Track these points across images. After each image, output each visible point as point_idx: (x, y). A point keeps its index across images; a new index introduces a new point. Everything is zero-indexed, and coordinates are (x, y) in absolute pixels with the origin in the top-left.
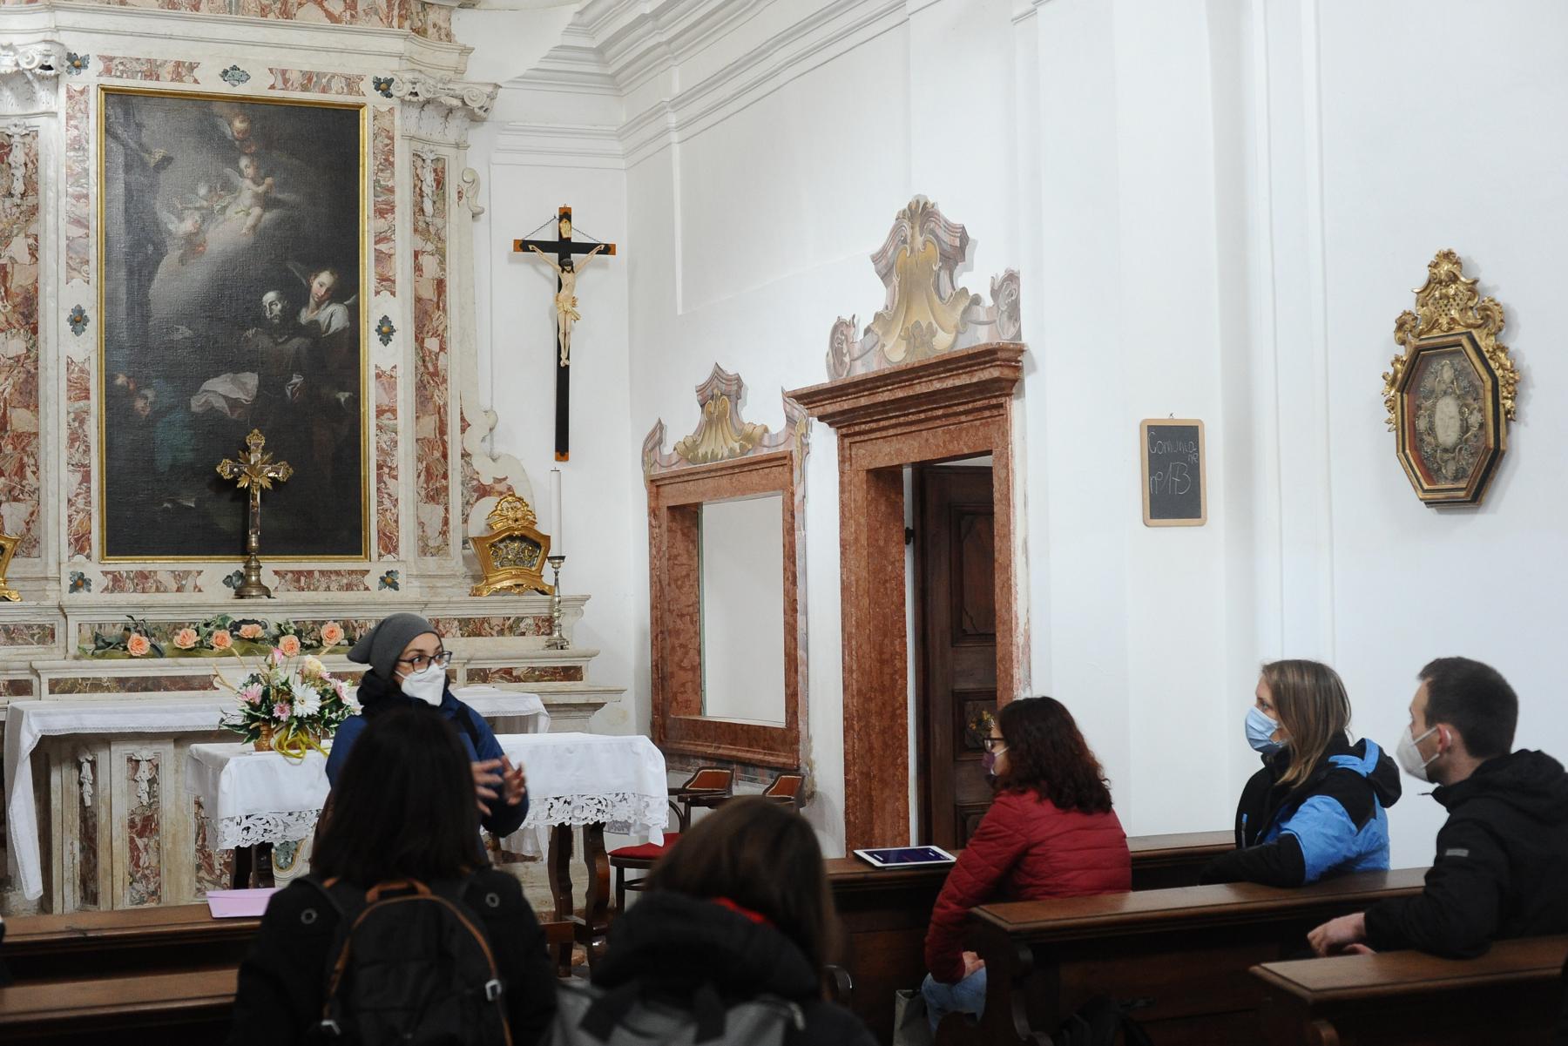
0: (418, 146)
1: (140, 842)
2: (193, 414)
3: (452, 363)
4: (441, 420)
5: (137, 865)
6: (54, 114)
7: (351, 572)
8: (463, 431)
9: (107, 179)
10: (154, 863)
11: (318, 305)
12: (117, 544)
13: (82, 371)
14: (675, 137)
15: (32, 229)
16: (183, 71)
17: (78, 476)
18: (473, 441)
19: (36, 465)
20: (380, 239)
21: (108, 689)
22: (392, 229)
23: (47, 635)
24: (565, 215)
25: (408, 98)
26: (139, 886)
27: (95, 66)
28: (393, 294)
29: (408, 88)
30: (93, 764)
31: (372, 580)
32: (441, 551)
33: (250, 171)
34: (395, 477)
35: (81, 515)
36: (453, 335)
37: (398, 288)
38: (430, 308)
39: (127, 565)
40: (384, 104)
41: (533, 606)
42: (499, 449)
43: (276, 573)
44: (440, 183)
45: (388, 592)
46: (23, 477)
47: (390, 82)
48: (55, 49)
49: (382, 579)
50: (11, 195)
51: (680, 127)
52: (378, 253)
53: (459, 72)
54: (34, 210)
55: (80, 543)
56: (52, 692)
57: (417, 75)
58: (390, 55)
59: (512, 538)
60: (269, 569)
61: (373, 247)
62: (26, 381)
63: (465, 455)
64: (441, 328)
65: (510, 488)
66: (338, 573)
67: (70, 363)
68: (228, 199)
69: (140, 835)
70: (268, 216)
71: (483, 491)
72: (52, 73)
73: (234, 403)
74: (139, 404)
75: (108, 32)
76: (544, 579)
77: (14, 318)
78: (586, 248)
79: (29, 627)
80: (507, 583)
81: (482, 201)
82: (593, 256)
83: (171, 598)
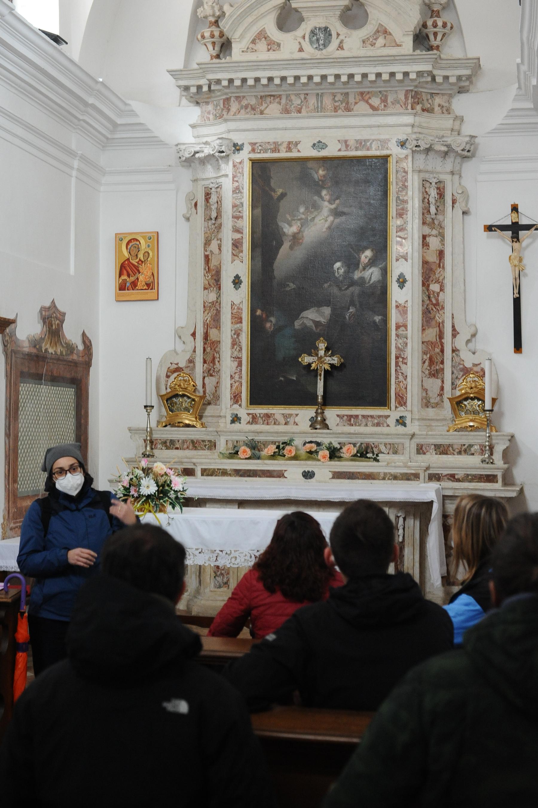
2: (295, 329)
4: (440, 331)
6: (226, 176)
7: (379, 417)
9: (254, 207)
11: (364, 269)
12: (256, 399)
13: (238, 308)
15: (219, 237)
16: (292, 146)
17: (236, 364)
18: (460, 342)
19: (219, 358)
21: (230, 475)
22: (406, 223)
23: (212, 445)
24: (515, 209)
25: (414, 149)
26: (219, 579)
27: (247, 148)
29: (415, 143)
31: (392, 421)
33: (327, 197)
34: (406, 364)
35: (237, 384)
36: (448, 283)
38: (434, 267)
41: (478, 438)
43: (338, 416)
44: (441, 195)
45: (400, 428)
46: (214, 364)
48: (225, 142)
49: (397, 420)
50: (211, 219)
55: (236, 398)
56: (202, 475)
57: (418, 135)
58: (406, 125)
60: (332, 414)
62: (216, 314)
63: (454, 351)
66: (372, 417)
68: (316, 213)
70: (337, 221)
72: (224, 154)
73: (317, 324)
74: (268, 325)
75: (258, 130)
77: (212, 282)
78: (528, 227)
83: (281, 428)
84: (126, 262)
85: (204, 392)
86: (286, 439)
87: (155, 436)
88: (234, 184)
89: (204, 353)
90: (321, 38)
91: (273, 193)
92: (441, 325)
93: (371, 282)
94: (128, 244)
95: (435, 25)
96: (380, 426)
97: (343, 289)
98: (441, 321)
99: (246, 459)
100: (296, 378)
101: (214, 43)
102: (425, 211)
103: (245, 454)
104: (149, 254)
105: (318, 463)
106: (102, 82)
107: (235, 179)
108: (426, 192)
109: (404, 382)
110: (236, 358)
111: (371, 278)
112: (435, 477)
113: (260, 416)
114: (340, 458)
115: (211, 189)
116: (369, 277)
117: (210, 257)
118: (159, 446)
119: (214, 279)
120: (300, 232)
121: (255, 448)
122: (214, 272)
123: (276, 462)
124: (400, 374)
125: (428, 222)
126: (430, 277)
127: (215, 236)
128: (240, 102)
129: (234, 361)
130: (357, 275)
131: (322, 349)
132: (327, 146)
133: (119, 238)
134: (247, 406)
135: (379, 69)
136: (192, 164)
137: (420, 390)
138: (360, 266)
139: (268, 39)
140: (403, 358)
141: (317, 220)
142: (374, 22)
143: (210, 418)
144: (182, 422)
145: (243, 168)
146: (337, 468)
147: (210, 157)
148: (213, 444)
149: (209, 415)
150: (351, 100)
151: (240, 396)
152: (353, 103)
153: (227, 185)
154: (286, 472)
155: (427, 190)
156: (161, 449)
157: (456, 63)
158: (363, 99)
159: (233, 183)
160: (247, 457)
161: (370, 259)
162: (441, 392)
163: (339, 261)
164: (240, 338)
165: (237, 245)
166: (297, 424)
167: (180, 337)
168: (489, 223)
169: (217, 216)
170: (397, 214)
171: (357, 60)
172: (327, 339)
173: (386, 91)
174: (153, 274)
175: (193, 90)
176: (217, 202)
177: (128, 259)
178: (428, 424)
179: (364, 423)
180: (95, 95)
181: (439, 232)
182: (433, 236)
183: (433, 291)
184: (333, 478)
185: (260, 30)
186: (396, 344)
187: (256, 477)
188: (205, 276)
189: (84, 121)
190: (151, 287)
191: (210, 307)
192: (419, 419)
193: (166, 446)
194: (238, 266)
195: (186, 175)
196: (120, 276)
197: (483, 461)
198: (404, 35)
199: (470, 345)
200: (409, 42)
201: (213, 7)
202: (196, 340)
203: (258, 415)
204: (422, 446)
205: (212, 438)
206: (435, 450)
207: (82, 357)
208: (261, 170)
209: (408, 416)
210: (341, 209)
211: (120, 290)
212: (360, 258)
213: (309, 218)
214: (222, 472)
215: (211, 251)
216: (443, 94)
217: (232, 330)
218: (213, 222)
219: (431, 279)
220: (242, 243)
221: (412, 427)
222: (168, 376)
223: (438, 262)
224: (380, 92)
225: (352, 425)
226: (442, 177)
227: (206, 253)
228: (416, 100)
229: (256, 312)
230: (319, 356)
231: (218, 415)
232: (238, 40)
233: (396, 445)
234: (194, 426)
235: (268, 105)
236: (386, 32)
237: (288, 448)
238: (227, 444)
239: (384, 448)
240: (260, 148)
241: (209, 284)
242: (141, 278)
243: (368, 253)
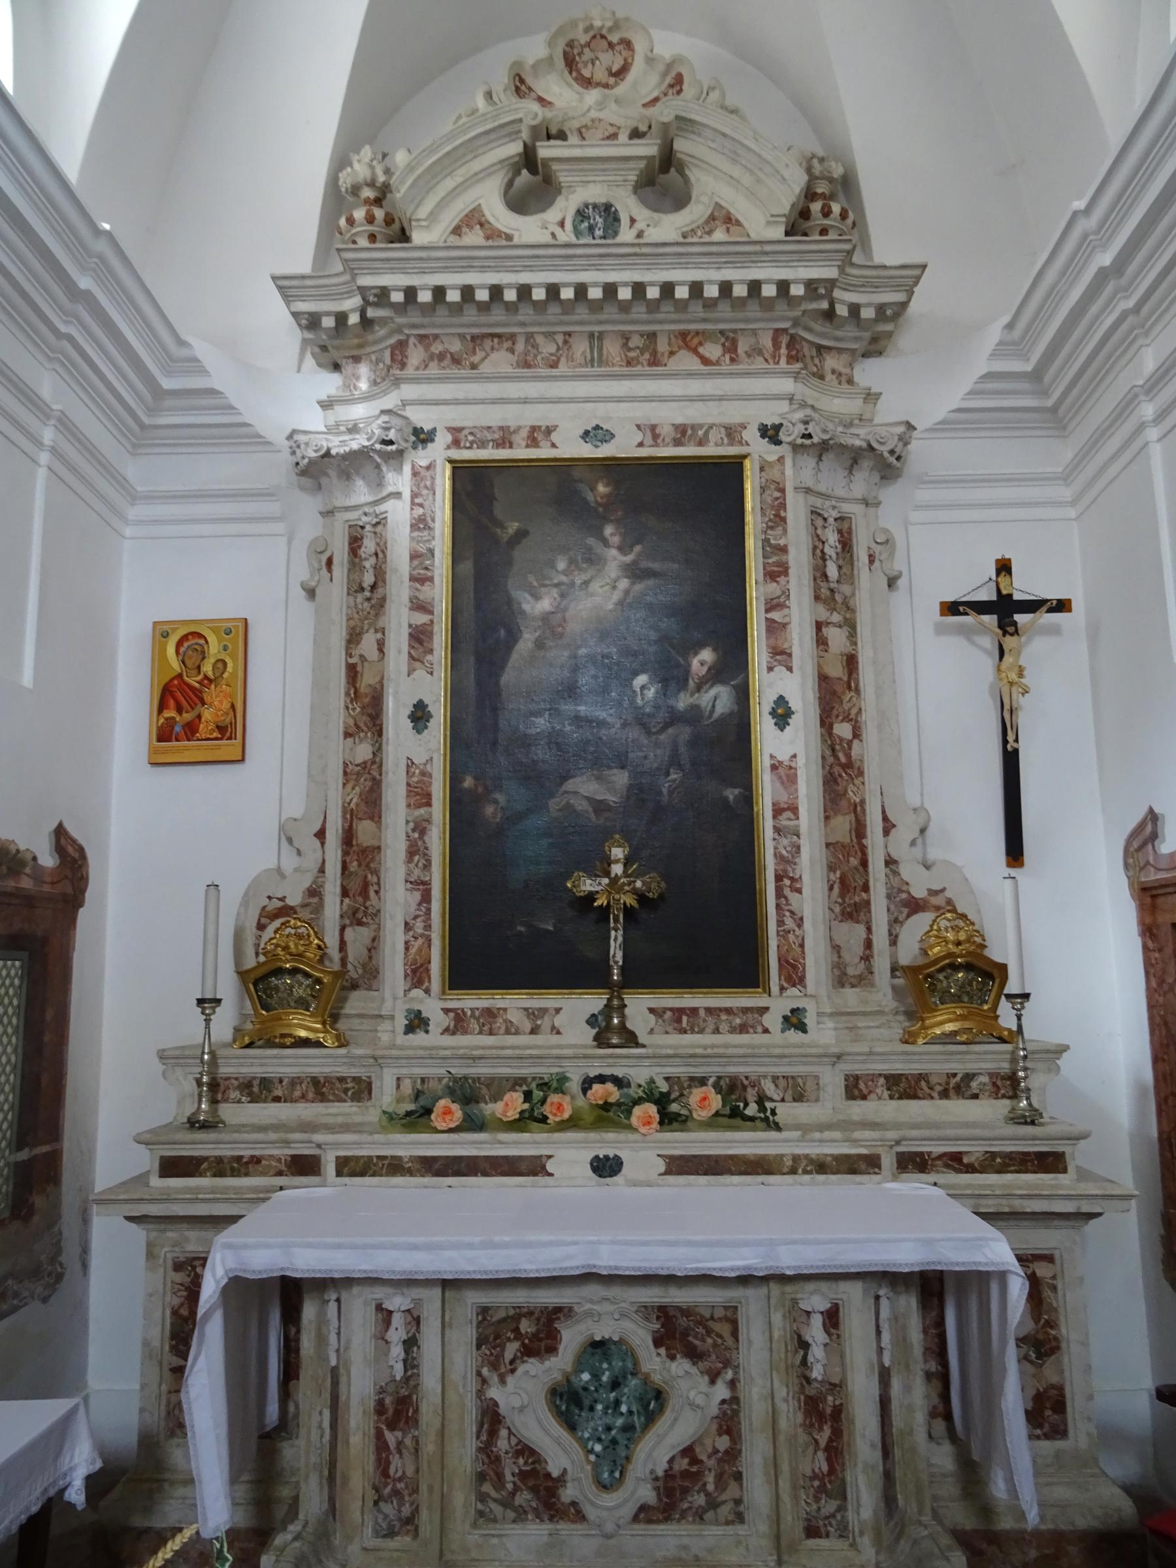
0: (818, 502)
1: (391, 1438)
3: (869, 751)
5: (385, 1474)
6: (397, 495)
7: (745, 1010)
8: (886, 832)
9: (456, 558)
10: (410, 1472)
11: (699, 688)
12: (462, 976)
13: (423, 774)
14: (1152, 434)
15: (380, 624)
16: (539, 436)
17: (417, 896)
18: (899, 844)
19: (378, 884)
21: (410, 1173)
22: (786, 594)
23: (362, 1090)
24: (1004, 567)
25: (799, 441)
26: (388, 1508)
27: (443, 438)
28: (790, 669)
29: (800, 429)
30: (338, 1300)
31: (772, 1021)
32: (864, 980)
33: (616, 540)
34: (799, 891)
35: (420, 941)
36: (869, 719)
37: (796, 662)
38: (839, 688)
39: (472, 1001)
40: (771, 453)
41: (988, 1059)
42: (934, 854)
43: (651, 1010)
44: (846, 544)
45: (793, 1036)
46: (366, 897)
47: (777, 428)
48: (395, 421)
49: (785, 1018)
50: (363, 589)
51: (1160, 417)
52: (771, 624)
54: (382, 603)
55: (417, 975)
56: (339, 1174)
59: (955, 967)
60: (639, 1007)
61: (763, 615)
62: (372, 790)
63: (890, 862)
64: (854, 711)
65: (949, 902)
66: (728, 1011)
67: (410, 764)
69: (392, 1427)
70: (639, 587)
71: (915, 906)
72: (394, 447)
73: (600, 806)
74: (489, 810)
76: (1001, 1022)
77: (363, 720)
78: (1032, 606)
79: (342, 1080)
80: (950, 1027)
81: (899, 564)
82: (1047, 618)
84: (176, 682)
85: (344, 961)
86: (545, 1071)
87: (224, 1070)
88: (413, 511)
89: (343, 874)
90: (599, 225)
91: (498, 530)
92: (859, 808)
93: (716, 715)
94: (179, 644)
96: (747, 1032)
97: (654, 730)
98: (858, 800)
99: (450, 1131)
100: (555, 927)
102: (818, 575)
103: (448, 1117)
104: (225, 664)
105: (631, 1136)
106: (109, 234)
107: (417, 501)
108: (818, 536)
109: (798, 932)
110: (418, 884)
111: (714, 706)
112: (914, 1161)
113: (473, 1015)
115: (362, 527)
116: (709, 708)
117: (359, 668)
118: (234, 1094)
119: (367, 711)
120: (559, 610)
121: (467, 1093)
122: (367, 700)
123: (526, 1136)
124: (787, 914)
125: (823, 596)
126: (833, 708)
127: (370, 625)
128: (427, 348)
129: (411, 890)
131: (617, 861)
132: (613, 436)
133: (161, 632)
134: (444, 993)
136: (324, 481)
137: (829, 948)
138: (691, 681)
139: (487, 226)
140: (792, 879)
141: (595, 586)
142: (705, 199)
143: (357, 1021)
144: (290, 1035)
145: (433, 478)
146: (675, 1148)
148: (364, 1085)
149: (353, 1012)
150: (662, 346)
151: (428, 970)
152: (667, 354)
153: (399, 514)
154: (551, 1161)
155: (819, 532)
156: (239, 1102)
158: (688, 347)
159: (412, 509)
160: (452, 1125)
161: (709, 669)
162: (868, 952)
163: (643, 672)
164: (426, 838)
165: (420, 637)
166: (558, 1033)
167: (290, 841)
169: (375, 583)
170: (765, 575)
172: (628, 837)
173: (734, 331)
174: (233, 707)
175: (328, 322)
176: (376, 554)
177: (180, 676)
178: (850, 1025)
179: (712, 1027)
180: (94, 270)
181: (845, 618)
182: (835, 625)
183: (839, 737)
184: (668, 1172)
185: (471, 207)
186: (776, 848)
187: (476, 1175)
188: (347, 708)
189: (71, 339)
190: (228, 734)
191: (358, 773)
192: (832, 1015)
193: (250, 1094)
194: (419, 683)
195: (309, 506)
196: (160, 711)
198: (768, 223)
201: (372, 168)
202: (326, 845)
203: (469, 1013)
204: (857, 1078)
206: (888, 1089)
207: (53, 883)
208: (473, 484)
209: (810, 1007)
210: (645, 564)
211: (159, 740)
212: (690, 666)
213: (578, 582)
214: (389, 1165)
215: (361, 656)
216: (840, 351)
217: (407, 822)
218: (367, 594)
219: (835, 712)
220: (432, 633)
221: (823, 1033)
222: (261, 927)
223: (845, 678)
224: (722, 332)
225: (685, 1032)
226: (847, 508)
227: (351, 661)
228: (794, 353)
229: (462, 781)
230: (613, 875)
231: (377, 1013)
232: (424, 223)
233: (800, 1081)
234: (318, 1044)
235: (488, 355)
236: (730, 219)
237: (554, 1098)
238: (398, 1087)
239: (772, 1087)
240: (471, 438)
241: (356, 724)
242: (207, 714)
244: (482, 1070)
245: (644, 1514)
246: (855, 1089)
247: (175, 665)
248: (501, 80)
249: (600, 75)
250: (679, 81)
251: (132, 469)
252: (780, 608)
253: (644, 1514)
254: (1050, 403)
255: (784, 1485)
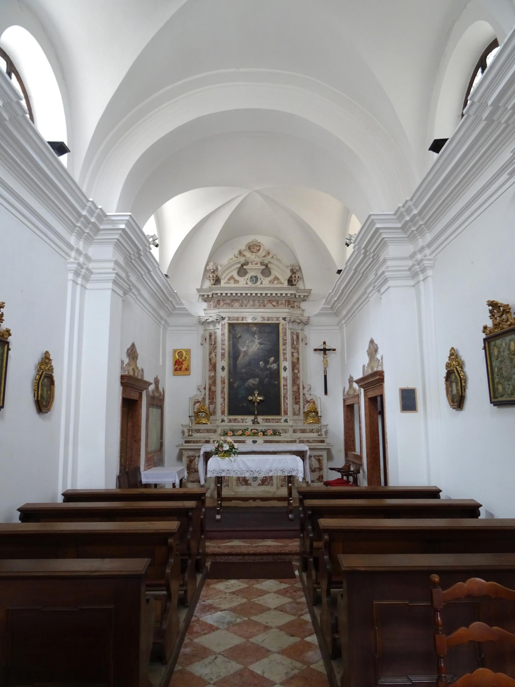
3: (301, 375)
6: (219, 329)
9: (229, 341)
11: (271, 364)
12: (230, 413)
20: (284, 350)
22: (286, 348)
23: (215, 431)
24: (325, 343)
27: (227, 319)
31: (282, 421)
33: (257, 338)
39: (232, 417)
40: (284, 322)
41: (315, 427)
42: (312, 393)
45: (286, 423)
51: (345, 323)
52: (283, 353)
53: (302, 315)
54: (216, 347)
55: (223, 413)
60: (260, 418)
63: (304, 394)
70: (261, 346)
73: (254, 384)
74: (235, 385)
77: (212, 368)
78: (329, 350)
82: (331, 351)
83: (241, 424)
86: (245, 428)
88: (221, 332)
95: (295, 277)
101: (213, 280)
114: (266, 435)
119: (213, 367)
130: (268, 366)
133: (175, 351)
135: (277, 292)
141: (253, 346)
147: (213, 321)
150: (266, 302)
157: (305, 291)
165: (223, 355)
168: (315, 348)
171: (269, 289)
172: (258, 390)
175: (206, 296)
194: (222, 363)
195: (201, 328)
197: (319, 435)
199: (309, 392)
200: (286, 283)
205: (214, 428)
208: (232, 326)
221: (290, 423)
222: (194, 405)
226: (298, 331)
237: (247, 431)
242: (184, 367)
243: (272, 358)
244: (234, 428)
245: (259, 485)
246: (294, 431)
247: (177, 357)
248: (237, 253)
249: (255, 251)
250: (269, 253)
251: (169, 320)
252: (286, 350)
253: (259, 485)
254: (335, 312)
255: (278, 481)
